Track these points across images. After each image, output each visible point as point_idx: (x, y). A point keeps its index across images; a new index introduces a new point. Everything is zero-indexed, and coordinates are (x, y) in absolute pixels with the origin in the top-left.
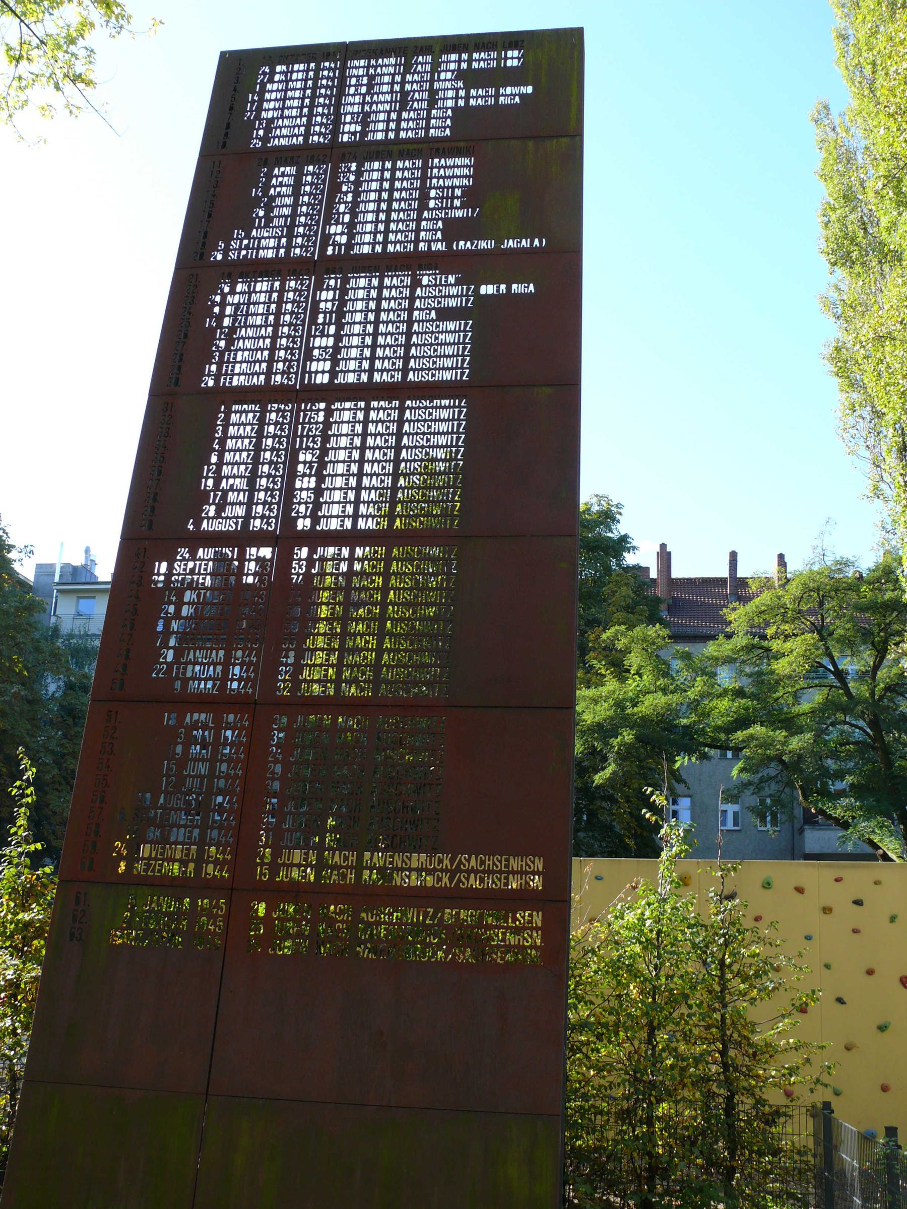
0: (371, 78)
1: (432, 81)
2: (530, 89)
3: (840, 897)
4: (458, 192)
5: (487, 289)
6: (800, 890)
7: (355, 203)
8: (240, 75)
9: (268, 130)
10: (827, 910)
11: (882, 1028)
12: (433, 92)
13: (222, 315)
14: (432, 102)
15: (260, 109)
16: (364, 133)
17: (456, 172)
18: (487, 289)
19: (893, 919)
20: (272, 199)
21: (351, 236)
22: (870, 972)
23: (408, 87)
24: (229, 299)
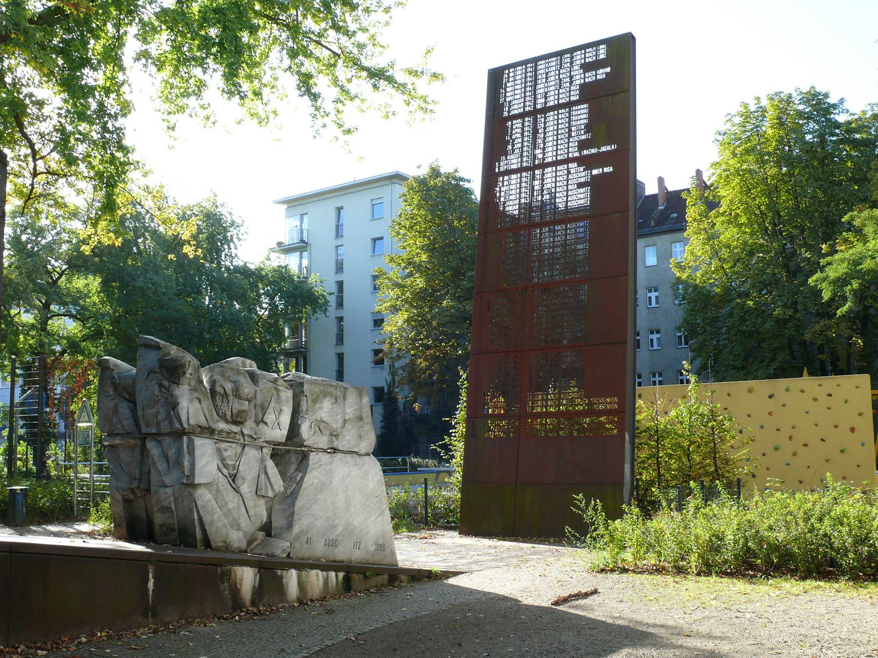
0: (547, 74)
1: (570, 71)
2: (608, 70)
3: (821, 393)
4: (583, 127)
5: (595, 172)
6: (802, 391)
7: (545, 138)
8: (496, 78)
9: (509, 107)
10: (815, 399)
11: (842, 451)
12: (571, 77)
13: (500, 196)
14: (571, 83)
15: (505, 97)
16: (546, 103)
17: (581, 114)
18: (595, 172)
19: (846, 402)
20: (514, 140)
21: (544, 154)
22: (836, 427)
23: (561, 76)
24: (502, 189)
